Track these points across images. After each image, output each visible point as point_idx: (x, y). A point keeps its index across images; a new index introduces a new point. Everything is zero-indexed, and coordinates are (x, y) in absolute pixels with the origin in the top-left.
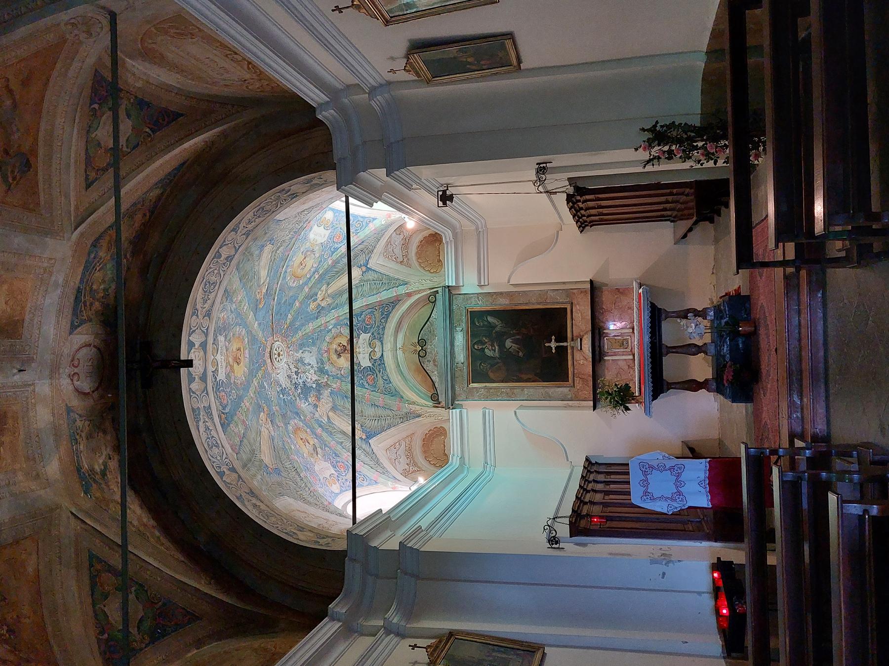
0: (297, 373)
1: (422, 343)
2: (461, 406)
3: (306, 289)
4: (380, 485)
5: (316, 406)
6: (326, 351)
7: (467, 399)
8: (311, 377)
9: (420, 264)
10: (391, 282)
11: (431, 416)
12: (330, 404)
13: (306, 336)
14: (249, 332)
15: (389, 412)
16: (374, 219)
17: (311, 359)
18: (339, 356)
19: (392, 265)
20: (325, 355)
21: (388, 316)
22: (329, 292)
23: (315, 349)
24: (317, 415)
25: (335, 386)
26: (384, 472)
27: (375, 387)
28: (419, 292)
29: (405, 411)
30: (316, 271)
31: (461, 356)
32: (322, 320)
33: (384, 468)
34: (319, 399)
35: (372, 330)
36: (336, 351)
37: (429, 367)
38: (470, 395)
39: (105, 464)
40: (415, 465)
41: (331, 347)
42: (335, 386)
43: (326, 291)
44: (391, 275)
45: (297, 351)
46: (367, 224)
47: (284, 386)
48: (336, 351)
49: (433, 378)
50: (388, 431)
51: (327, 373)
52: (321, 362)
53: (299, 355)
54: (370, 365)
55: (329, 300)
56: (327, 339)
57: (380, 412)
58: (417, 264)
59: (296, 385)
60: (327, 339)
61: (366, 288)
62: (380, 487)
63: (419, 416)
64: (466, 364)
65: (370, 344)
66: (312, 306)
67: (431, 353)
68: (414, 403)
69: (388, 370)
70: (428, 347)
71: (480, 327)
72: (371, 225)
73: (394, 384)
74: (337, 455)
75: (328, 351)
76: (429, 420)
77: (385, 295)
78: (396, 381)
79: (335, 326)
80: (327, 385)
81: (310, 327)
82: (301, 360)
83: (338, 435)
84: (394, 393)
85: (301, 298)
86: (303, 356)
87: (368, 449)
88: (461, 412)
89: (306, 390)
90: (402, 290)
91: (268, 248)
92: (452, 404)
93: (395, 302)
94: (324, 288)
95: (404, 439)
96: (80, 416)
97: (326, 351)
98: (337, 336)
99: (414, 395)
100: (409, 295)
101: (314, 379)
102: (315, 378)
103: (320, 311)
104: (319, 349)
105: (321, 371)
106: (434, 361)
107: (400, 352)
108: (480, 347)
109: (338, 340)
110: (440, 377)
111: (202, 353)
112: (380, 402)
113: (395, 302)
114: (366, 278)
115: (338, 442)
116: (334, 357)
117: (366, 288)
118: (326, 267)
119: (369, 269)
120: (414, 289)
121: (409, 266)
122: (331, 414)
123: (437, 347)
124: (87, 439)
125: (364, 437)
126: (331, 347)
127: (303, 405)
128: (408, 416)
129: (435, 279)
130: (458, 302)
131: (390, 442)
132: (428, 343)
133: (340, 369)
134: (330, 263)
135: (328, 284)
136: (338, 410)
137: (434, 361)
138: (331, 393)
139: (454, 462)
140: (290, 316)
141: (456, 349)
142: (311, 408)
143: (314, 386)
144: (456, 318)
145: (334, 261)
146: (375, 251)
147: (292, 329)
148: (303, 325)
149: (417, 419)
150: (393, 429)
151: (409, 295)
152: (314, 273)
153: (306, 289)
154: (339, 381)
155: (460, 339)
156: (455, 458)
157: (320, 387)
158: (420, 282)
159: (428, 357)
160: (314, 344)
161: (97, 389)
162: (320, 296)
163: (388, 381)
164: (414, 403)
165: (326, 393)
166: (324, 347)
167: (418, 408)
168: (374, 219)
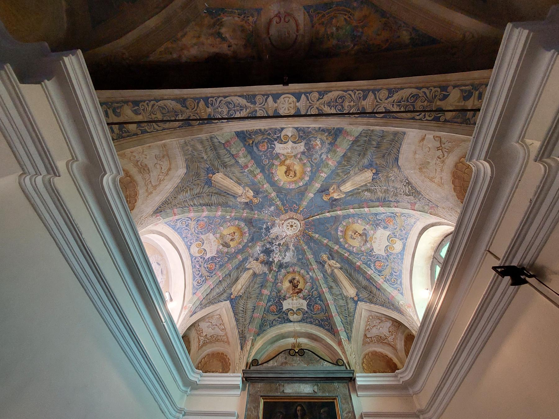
0: (279, 245)
1: (302, 352)
2: (244, 389)
3: (336, 247)
4: (191, 296)
5: (257, 260)
6: (294, 270)
7: (249, 395)
8: (276, 257)
9: (368, 354)
10: (349, 324)
11: (240, 359)
12: (258, 272)
13: (304, 253)
14: (307, 185)
15: (248, 321)
16: (402, 294)
17: (289, 257)
18: (291, 282)
19: (362, 332)
20: (291, 270)
21: (320, 325)
22: (336, 270)
23: (295, 261)
24: (251, 259)
25: (270, 276)
26: (202, 306)
27: (268, 311)
28: (344, 352)
29: (248, 336)
30: (351, 253)
31: (290, 389)
32: (315, 266)
33: (206, 306)
34: (262, 263)
35: (309, 311)
36: (294, 279)
37: (281, 359)
38: (253, 399)
39: (224, 39)
40: (205, 344)
41: (297, 274)
42: (270, 276)
43: (336, 268)
44: (354, 325)
45: (294, 245)
46: (396, 289)
47: (271, 231)
48: (294, 279)
49: (271, 362)
50: (233, 319)
51: (279, 271)
52: (287, 266)
53: (291, 247)
54: (284, 309)
55: (329, 271)
56: (302, 271)
57: (249, 313)
58: (366, 351)
59: (271, 243)
60: (302, 271)
61: (342, 303)
62: (189, 295)
63: (242, 349)
64: (283, 395)
65: (299, 309)
66: (325, 257)
67: (293, 360)
68: (253, 345)
69: (280, 326)
70: (298, 358)
71: (320, 413)
72: (396, 292)
73: (269, 330)
74: (221, 266)
75: (294, 272)
76: (237, 356)
77: (337, 320)
78: (272, 333)
79: (311, 278)
80: (270, 270)
81: (310, 256)
82: (288, 249)
83: (236, 274)
84: (261, 330)
85: (330, 244)
86: (291, 250)
87: (223, 297)
88: (235, 387)
89: (268, 252)
90: (343, 336)
91: (368, 175)
92: (247, 379)
93: (332, 330)
94: (338, 265)
95: (226, 334)
96: (255, 22)
97: (294, 270)
98: (304, 279)
99: (258, 347)
100: (340, 343)
101: (275, 259)
102: (276, 260)
103: (321, 264)
104: (295, 264)
105: (281, 266)
106: (286, 363)
107: (291, 340)
108: (299, 413)
109: (301, 281)
110: (272, 367)
111: (292, 112)
112: (256, 315)
113: (332, 330)
114: (349, 301)
115: (230, 271)
116: (290, 277)
117: (342, 303)
118: (354, 261)
119: (356, 303)
120: (345, 348)
121: (364, 343)
122: (251, 271)
123: (299, 365)
124: (242, 26)
125: (232, 296)
126: (297, 274)
127: (258, 248)
128: (243, 338)
129: (358, 367)
130: (340, 388)
131: (225, 319)
132: (301, 358)
133: (281, 282)
134: (358, 264)
135: (341, 268)
136: (254, 278)
137: (286, 363)
138: (265, 273)
139: (194, 376)
140: (317, 236)
141: (296, 385)
142: (256, 255)
143: (271, 260)
144: (326, 385)
145: (359, 267)
146: (372, 305)
147: (309, 239)
148: (311, 249)
149: (239, 347)
150: (235, 323)
151: (340, 343)
152: (349, 251)
153: (336, 247)
154: (273, 281)
155: (306, 389)
156: (199, 376)
157: (268, 264)
158: (352, 353)
159: (289, 358)
160: (299, 260)
161: (271, 43)
162: (332, 262)
163: (272, 325)
164: (253, 345)
165: (266, 269)
166: (297, 269)
167: (248, 348)
168: (402, 294)
